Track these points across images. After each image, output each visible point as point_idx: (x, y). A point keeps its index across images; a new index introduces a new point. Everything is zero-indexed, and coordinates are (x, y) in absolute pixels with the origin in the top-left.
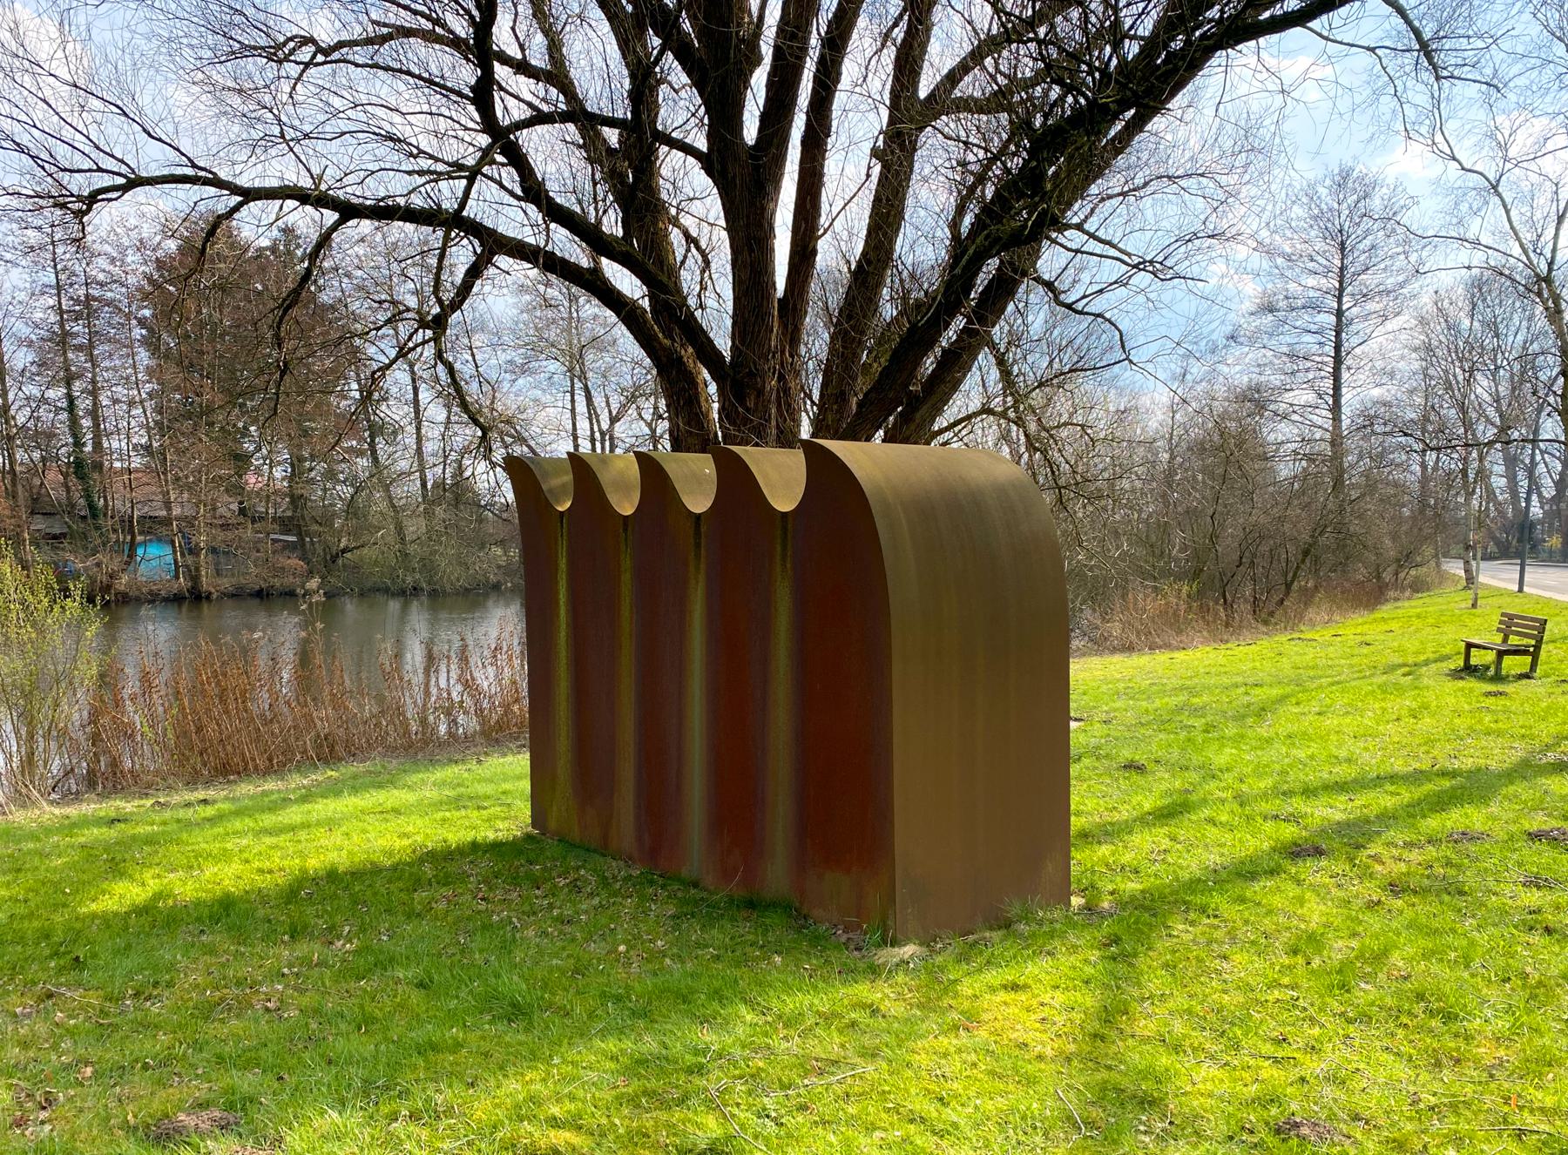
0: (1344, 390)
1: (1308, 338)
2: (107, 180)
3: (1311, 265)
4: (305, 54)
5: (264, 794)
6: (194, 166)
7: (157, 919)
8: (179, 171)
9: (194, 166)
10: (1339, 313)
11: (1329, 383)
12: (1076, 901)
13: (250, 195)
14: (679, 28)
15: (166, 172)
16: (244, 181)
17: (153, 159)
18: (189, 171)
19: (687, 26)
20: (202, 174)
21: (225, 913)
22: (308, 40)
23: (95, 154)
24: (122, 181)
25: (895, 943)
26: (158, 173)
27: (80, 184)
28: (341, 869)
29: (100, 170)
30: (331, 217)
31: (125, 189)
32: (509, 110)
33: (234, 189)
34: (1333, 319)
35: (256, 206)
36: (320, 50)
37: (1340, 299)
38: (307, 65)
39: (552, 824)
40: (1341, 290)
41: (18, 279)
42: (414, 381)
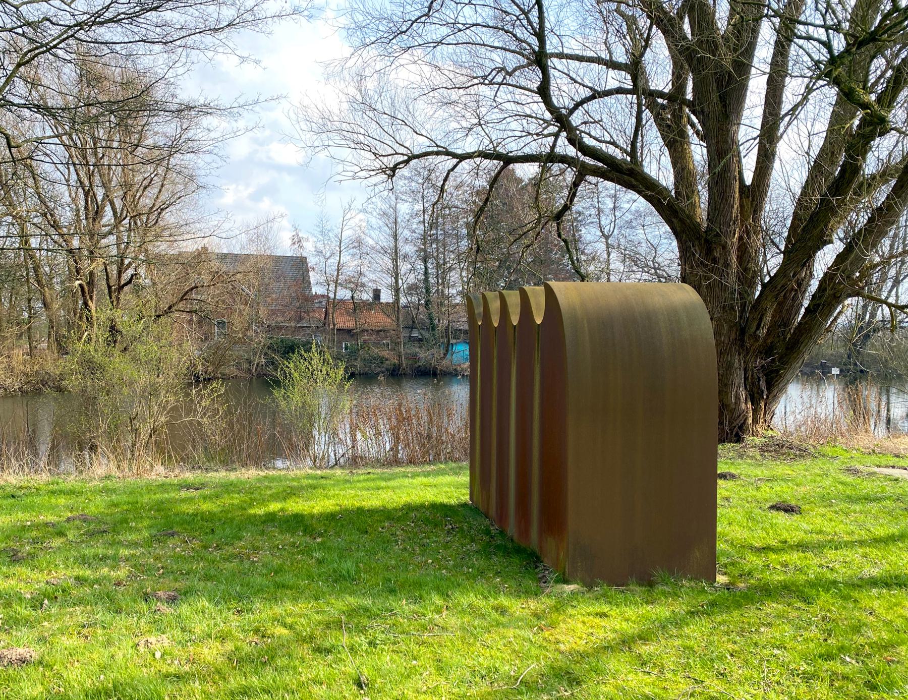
5: (384, 473)
6: (437, 146)
7: (271, 518)
8: (430, 149)
9: (437, 146)
12: (721, 579)
13: (462, 158)
14: (681, 29)
15: (424, 151)
16: (459, 152)
17: (419, 144)
18: (435, 149)
19: (687, 27)
20: (440, 149)
21: (297, 522)
23: (396, 146)
24: (406, 158)
25: (566, 582)
27: (391, 162)
30: (455, 161)
31: (406, 162)
32: (564, 93)
33: (454, 155)
35: (466, 165)
39: (475, 500)
41: (907, 291)
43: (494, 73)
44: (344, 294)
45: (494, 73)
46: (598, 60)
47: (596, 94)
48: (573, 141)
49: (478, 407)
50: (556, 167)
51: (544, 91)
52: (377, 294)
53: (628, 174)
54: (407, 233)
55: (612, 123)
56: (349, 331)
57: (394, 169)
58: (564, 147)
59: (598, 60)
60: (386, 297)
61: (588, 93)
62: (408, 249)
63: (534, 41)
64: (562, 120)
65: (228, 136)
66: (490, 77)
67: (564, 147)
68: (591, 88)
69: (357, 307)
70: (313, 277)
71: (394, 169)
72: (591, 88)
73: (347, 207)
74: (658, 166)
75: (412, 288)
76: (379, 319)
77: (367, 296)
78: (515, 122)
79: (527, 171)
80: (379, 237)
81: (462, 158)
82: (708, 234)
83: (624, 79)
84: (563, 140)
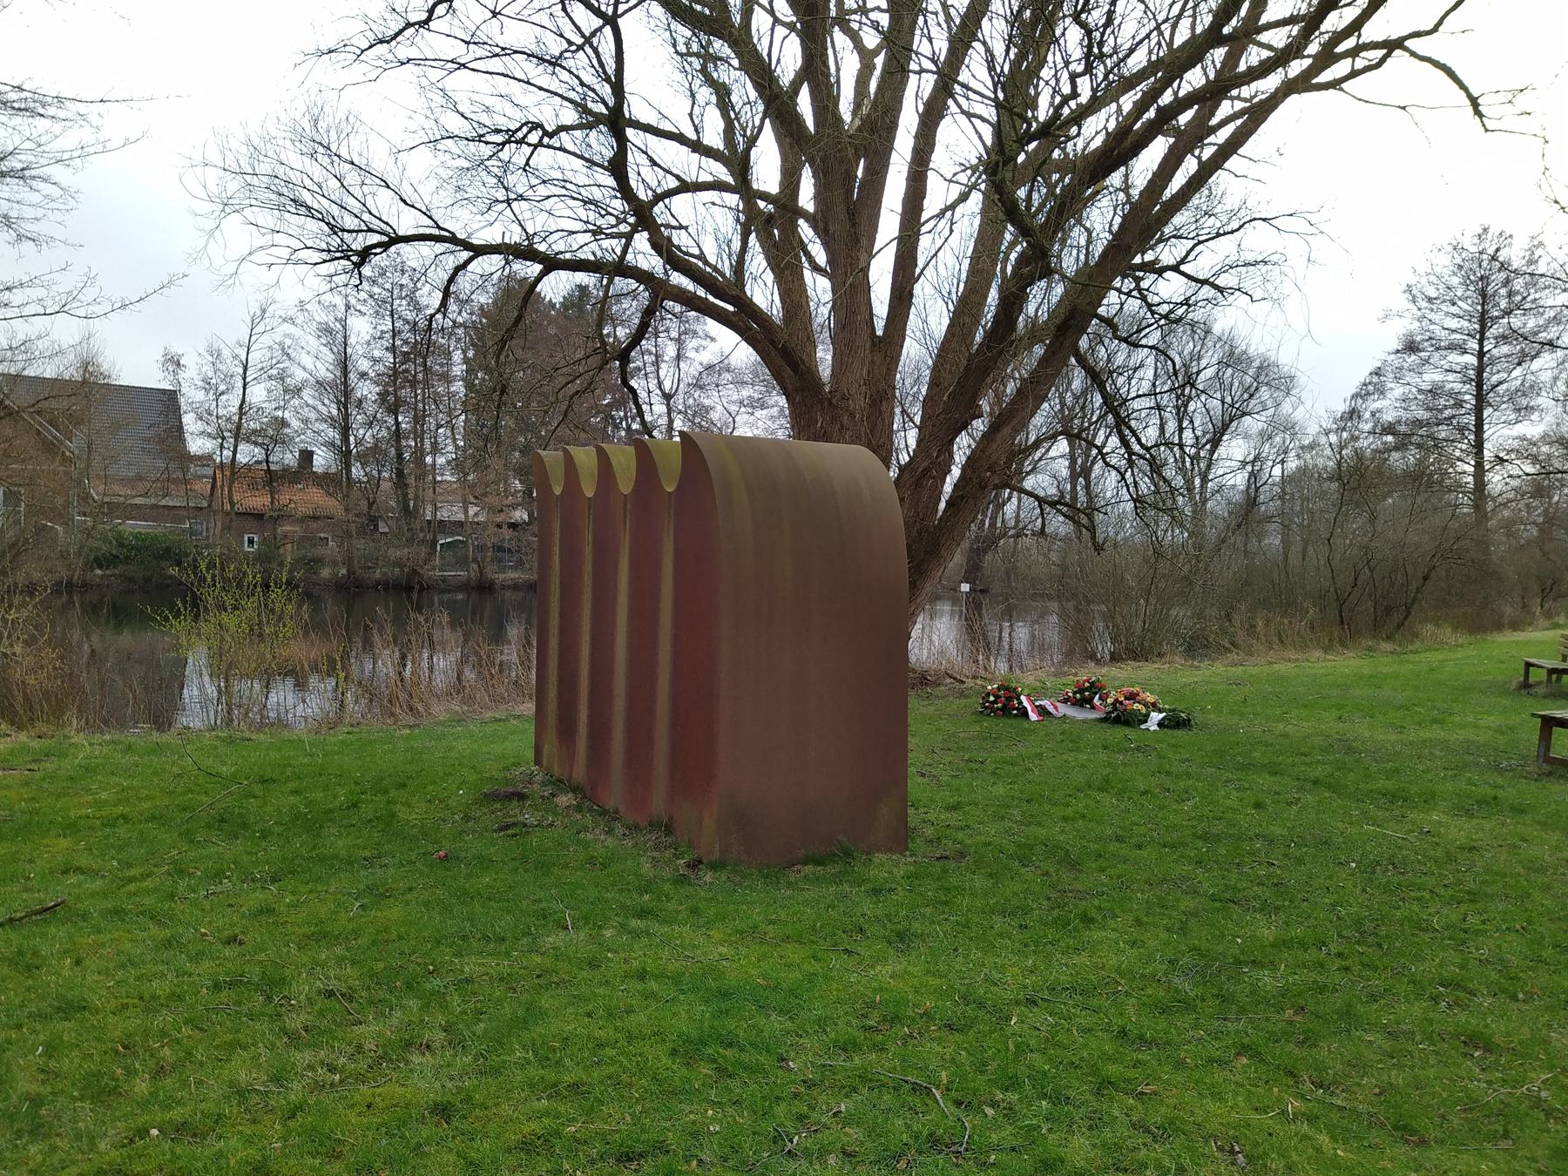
0: (1486, 427)
1: (1451, 377)
2: (375, 238)
3: (1454, 310)
4: (534, 138)
6: (439, 227)
8: (428, 231)
9: (439, 227)
10: (1481, 354)
11: (1471, 420)
13: (479, 251)
18: (436, 232)
22: (536, 126)
23: (366, 217)
26: (409, 233)
27: (358, 243)
28: (1318, 653)
29: (370, 230)
30: (465, 255)
31: (385, 246)
33: (466, 245)
34: (1473, 360)
36: (546, 133)
37: (1481, 343)
38: (536, 147)
40: (1482, 332)
42: (669, 413)
43: (525, 130)
44: (247, 454)
45: (525, 130)
46: (680, 138)
47: (685, 187)
48: (662, 246)
49: (587, 580)
50: (622, 284)
51: (618, 167)
52: (307, 456)
53: (725, 298)
54: (364, 365)
55: (707, 225)
56: (258, 517)
57: (365, 254)
58: (643, 253)
59: (680, 138)
60: (322, 460)
61: (672, 183)
62: (366, 390)
63: (606, 91)
64: (642, 215)
65: (92, 150)
66: (520, 135)
67: (643, 253)
68: (678, 177)
69: (273, 478)
70: (189, 421)
71: (365, 254)
72: (678, 177)
73: (258, 313)
74: (764, 293)
75: (373, 454)
76: (310, 499)
77: (290, 459)
78: (562, 207)
79: (557, 287)
80: (315, 362)
81: (479, 251)
82: (829, 383)
83: (722, 172)
84: (641, 240)
